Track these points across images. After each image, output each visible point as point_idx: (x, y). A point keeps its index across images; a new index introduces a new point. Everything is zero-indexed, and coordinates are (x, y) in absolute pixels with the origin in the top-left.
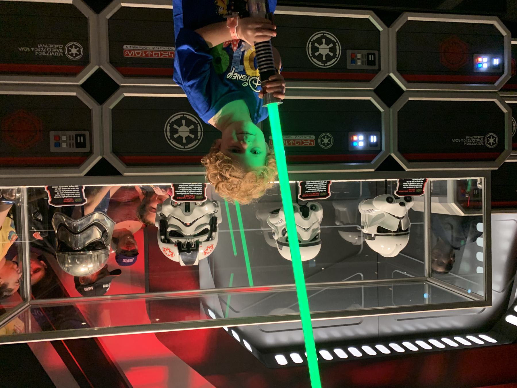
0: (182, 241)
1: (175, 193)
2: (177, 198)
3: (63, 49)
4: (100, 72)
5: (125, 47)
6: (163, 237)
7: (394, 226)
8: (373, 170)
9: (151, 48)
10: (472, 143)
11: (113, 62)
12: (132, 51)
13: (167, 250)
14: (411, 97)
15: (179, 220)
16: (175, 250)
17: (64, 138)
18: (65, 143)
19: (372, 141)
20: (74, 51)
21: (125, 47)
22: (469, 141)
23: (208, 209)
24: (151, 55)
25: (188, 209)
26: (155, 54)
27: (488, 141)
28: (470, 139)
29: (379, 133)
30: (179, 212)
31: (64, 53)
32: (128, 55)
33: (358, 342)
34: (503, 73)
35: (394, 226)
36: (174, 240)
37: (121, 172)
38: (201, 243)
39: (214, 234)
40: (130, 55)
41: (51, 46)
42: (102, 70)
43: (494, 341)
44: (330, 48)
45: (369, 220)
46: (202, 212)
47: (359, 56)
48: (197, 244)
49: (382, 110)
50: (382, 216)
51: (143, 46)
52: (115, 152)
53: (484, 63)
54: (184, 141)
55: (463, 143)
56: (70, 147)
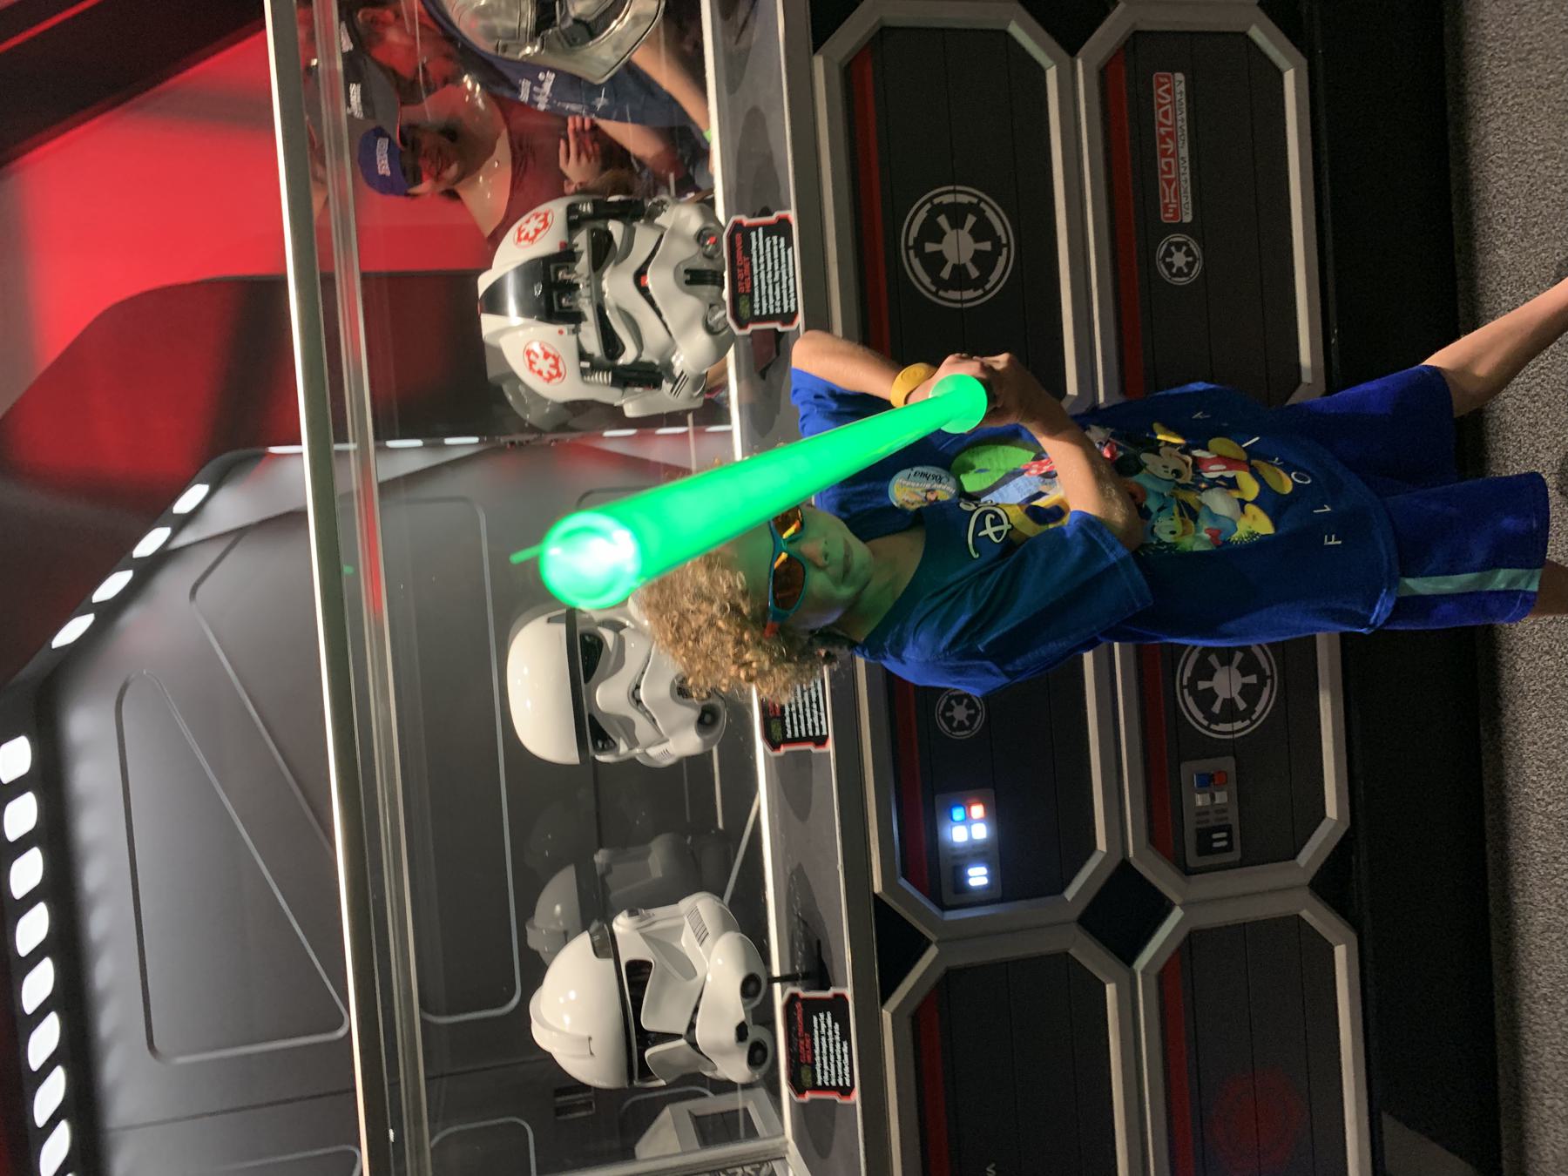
0: (583, 264)
1: (755, 228)
2: (738, 236)
6: (587, 208)
8: (877, 887)
9: (1184, 152)
11: (1137, 40)
12: (1172, 97)
14: (1119, 992)
16: (547, 244)
21: (1180, 77)
24: (1164, 153)
26: (1168, 164)
29: (999, 895)
30: (683, 251)
33: (78, 1052)
36: (582, 240)
38: (576, 331)
40: (1160, 91)
44: (1232, 700)
45: (663, 930)
47: (1221, 798)
48: (575, 318)
49: (1070, 893)
50: (688, 970)
52: (883, 34)
56: (1198, 814)
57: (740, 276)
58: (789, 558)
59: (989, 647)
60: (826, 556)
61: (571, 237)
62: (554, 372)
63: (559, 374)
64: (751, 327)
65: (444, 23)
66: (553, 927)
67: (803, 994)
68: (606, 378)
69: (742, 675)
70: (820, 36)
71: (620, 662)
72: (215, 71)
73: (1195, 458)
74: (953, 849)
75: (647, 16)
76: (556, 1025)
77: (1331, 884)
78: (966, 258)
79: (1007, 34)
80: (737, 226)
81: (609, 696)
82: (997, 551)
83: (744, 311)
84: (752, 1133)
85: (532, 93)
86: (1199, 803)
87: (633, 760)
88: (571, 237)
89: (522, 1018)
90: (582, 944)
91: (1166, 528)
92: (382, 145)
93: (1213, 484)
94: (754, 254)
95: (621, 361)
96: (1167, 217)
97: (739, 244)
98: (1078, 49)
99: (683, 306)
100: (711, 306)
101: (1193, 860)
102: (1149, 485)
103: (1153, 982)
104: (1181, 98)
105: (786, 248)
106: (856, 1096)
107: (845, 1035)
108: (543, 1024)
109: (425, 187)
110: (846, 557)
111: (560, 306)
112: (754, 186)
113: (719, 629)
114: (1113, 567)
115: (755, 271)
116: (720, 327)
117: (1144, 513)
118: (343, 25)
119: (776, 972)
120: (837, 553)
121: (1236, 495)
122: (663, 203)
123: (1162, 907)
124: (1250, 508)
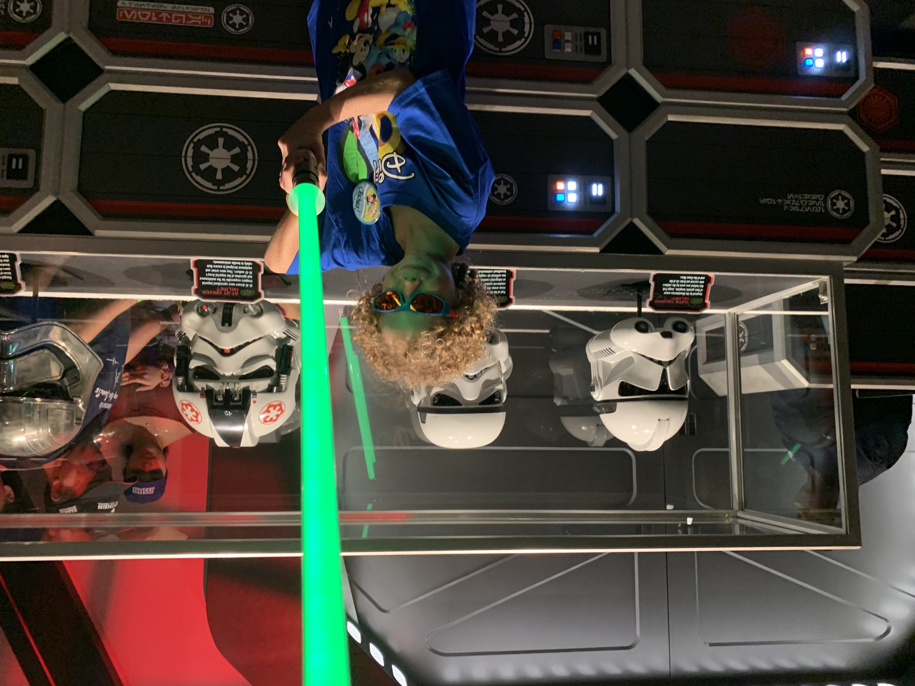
0: (215, 385)
1: (199, 282)
2: (204, 292)
3: (825, 201)
4: (67, 46)
6: (180, 380)
7: (651, 379)
8: (596, 250)
9: (169, 7)
10: (800, 207)
11: (94, 28)
13: (187, 405)
15: (211, 344)
16: (201, 405)
19: (594, 193)
20: (841, 204)
22: (794, 203)
26: (176, 18)
27: (834, 204)
28: (797, 199)
30: (211, 326)
31: (825, 208)
32: (124, 16)
34: (857, 78)
35: (651, 379)
36: (200, 385)
38: (255, 393)
41: (807, 196)
42: (75, 45)
47: (568, 36)
48: (246, 393)
49: (614, 136)
50: (629, 361)
52: (82, 190)
54: (219, 176)
55: (782, 205)
57: (228, 293)
58: (412, 303)
59: (472, 172)
60: (414, 279)
62: (278, 408)
63: (280, 405)
64: (260, 290)
66: (594, 432)
67: (651, 299)
68: (284, 378)
69: (478, 332)
70: (84, 231)
72: (82, 586)
73: (359, 32)
74: (580, 202)
75: (62, 333)
76: (650, 437)
78: (227, 154)
79: (85, 113)
80: (197, 292)
81: (470, 393)
83: (250, 293)
84: (722, 330)
85: (107, 402)
86: (570, 50)
87: (507, 381)
89: (643, 456)
90: (606, 419)
91: (400, 54)
92: (136, 490)
93: (375, 22)
95: (275, 369)
96: (210, 23)
97: (209, 292)
98: (99, 67)
99: (244, 329)
100: (245, 312)
101: (603, 58)
102: (373, 60)
105: (213, 264)
106: (712, 274)
107: (677, 277)
109: (162, 466)
110: (414, 268)
112: (175, 278)
113: (451, 344)
115: (226, 284)
116: (258, 308)
117: (390, 67)
118: (61, 510)
119: (635, 310)
120: (412, 273)
121: (383, 9)
122: (180, 334)
123: (628, 80)
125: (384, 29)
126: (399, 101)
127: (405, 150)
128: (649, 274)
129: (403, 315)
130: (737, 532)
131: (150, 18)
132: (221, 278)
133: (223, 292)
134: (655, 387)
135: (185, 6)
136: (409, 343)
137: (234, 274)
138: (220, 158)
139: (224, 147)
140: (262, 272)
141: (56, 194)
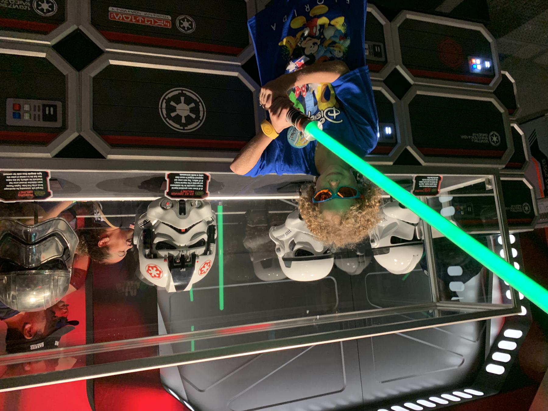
1: (170, 187)
2: (172, 194)
3: (488, 137)
5: (110, 9)
6: (147, 251)
8: (391, 163)
9: (143, 14)
10: (478, 140)
11: (94, 23)
14: (419, 90)
16: (164, 266)
17: (27, 107)
18: (29, 113)
23: (206, 213)
25: (183, 211)
26: (148, 21)
29: (392, 124)
30: (172, 216)
31: (31, 7)
34: (494, 75)
36: (163, 253)
37: (104, 155)
39: (213, 247)
41: (481, 135)
43: (481, 394)
46: (200, 217)
48: (194, 256)
49: (393, 101)
50: (394, 224)
51: (133, 11)
52: (96, 128)
53: (478, 64)
56: (35, 119)
61: (161, 257)
65: (483, 287)
71: (307, 243)
77: (391, 16)
78: (187, 107)
81: (319, 248)
82: (343, 113)
88: (161, 257)
91: (338, 54)
93: (322, 33)
94: (180, 188)
95: (206, 240)
97: (175, 194)
102: (321, 53)
103: (418, 79)
104: (119, 10)
105: (179, 176)
107: (426, 177)
108: (355, 272)
111: (179, 263)
112: (154, 184)
114: (361, 75)
115: (186, 188)
124: (333, 22)
125: (328, 38)
126: (344, 77)
127: (340, 106)
128: (412, 177)
129: (336, 201)
130: (437, 316)
131: (131, 20)
132: (184, 184)
133: (184, 193)
134: (411, 238)
135: (152, 14)
136: (342, 217)
137: (192, 182)
138: (183, 110)
139: (177, 104)
140: (210, 180)
141: (78, 131)
